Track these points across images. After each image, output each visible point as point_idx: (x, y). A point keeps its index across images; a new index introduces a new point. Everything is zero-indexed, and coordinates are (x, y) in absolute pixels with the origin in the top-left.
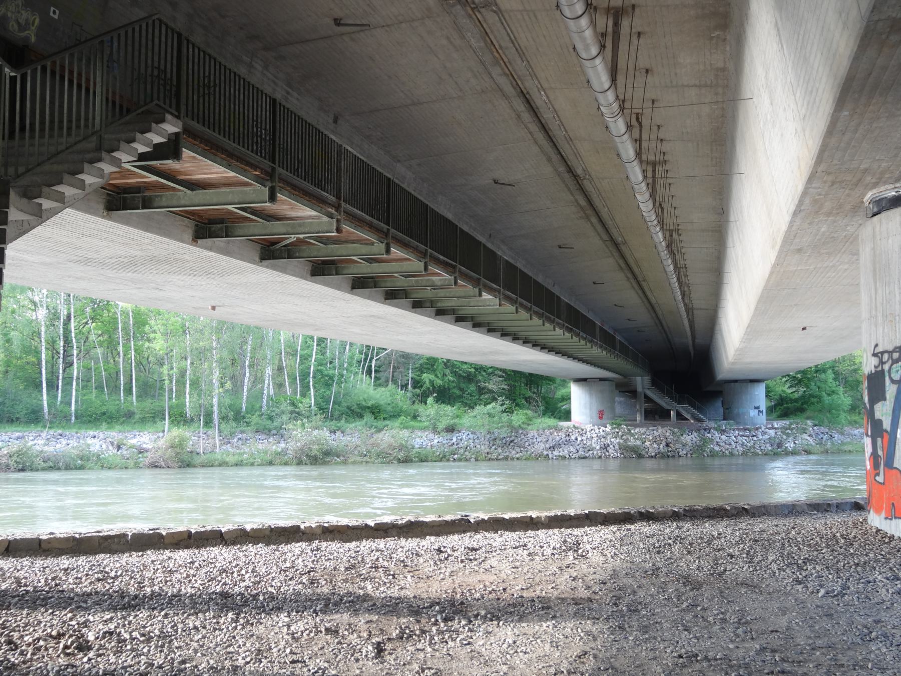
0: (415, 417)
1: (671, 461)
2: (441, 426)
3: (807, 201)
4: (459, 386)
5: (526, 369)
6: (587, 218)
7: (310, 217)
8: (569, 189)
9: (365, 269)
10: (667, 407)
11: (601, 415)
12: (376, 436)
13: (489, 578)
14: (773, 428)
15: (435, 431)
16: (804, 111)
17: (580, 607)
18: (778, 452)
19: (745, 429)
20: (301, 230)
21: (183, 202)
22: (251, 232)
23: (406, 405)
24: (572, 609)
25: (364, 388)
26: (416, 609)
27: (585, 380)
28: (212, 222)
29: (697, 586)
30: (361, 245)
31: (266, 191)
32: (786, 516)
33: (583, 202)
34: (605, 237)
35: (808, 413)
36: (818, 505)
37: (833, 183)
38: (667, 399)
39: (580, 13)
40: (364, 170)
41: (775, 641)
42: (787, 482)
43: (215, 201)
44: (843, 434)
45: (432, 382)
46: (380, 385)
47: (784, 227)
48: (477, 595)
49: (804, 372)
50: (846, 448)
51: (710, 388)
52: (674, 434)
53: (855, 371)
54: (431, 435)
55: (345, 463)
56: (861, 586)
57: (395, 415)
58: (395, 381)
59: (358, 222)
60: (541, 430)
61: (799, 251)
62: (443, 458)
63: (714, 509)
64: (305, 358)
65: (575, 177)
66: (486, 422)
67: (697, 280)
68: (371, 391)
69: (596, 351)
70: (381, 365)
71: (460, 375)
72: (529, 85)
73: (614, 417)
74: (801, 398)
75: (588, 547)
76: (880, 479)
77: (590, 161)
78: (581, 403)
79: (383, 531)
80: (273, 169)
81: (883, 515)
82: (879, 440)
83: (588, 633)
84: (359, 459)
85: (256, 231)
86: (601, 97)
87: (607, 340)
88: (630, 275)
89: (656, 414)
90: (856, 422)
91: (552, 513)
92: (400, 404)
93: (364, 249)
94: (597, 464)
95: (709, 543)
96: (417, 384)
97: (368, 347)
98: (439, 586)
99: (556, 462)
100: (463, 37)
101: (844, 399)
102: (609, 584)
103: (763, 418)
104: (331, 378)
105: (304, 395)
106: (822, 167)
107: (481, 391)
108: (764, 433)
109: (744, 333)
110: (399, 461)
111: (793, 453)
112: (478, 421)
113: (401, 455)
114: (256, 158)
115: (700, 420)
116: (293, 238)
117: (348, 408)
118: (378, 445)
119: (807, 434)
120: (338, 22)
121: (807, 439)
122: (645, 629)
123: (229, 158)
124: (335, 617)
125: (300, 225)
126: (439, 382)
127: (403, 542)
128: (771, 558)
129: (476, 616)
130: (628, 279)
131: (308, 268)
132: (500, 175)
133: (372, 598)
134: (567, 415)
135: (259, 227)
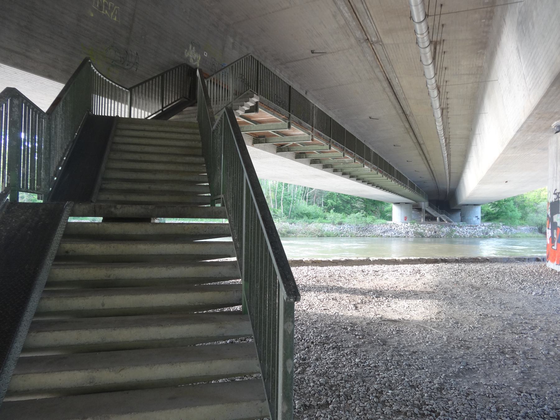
0: (325, 218)
1: (437, 239)
2: (336, 222)
3: (525, 126)
4: (343, 205)
5: (373, 198)
6: (409, 133)
7: (300, 134)
8: (402, 121)
9: (317, 155)
10: (435, 216)
11: (406, 219)
12: (309, 226)
13: (388, 282)
14: (484, 226)
15: (334, 224)
16: (530, 87)
17: (430, 295)
18: (486, 236)
19: (471, 226)
20: (297, 140)
21: (252, 129)
22: (276, 141)
23: (321, 213)
24: (428, 296)
25: (303, 206)
26: (364, 293)
27: (399, 203)
28: (260, 137)
29: (478, 289)
30: (321, 146)
31: (287, 124)
32: (506, 263)
33: (407, 126)
34: (415, 141)
35: (500, 219)
36: (520, 258)
37: (539, 118)
38: (435, 212)
39: (427, 45)
40: (321, 114)
41: (519, 311)
42: (488, 249)
43: (265, 128)
44: (516, 229)
45: (332, 204)
46: (310, 204)
47: (510, 137)
48: (386, 289)
49: (499, 201)
50: (518, 235)
51: (455, 208)
52: (438, 227)
53: (524, 201)
54: (332, 226)
55: (296, 236)
56: (550, 292)
57: (316, 217)
58: (316, 203)
59: (319, 136)
60: (379, 225)
61: (515, 147)
62: (337, 235)
63: (474, 259)
64: (279, 193)
65: (406, 115)
66: (356, 221)
67: (455, 160)
68: (306, 207)
69: (407, 191)
70: (310, 196)
71: (344, 201)
72: (391, 76)
73: (412, 219)
74: (498, 213)
75: (425, 272)
76: (555, 247)
77: (415, 109)
78: (397, 213)
79: (335, 263)
80: (290, 115)
81: (555, 263)
82: (555, 231)
83: (438, 305)
84: (302, 235)
85: (278, 141)
86: (429, 82)
87: (412, 186)
88: (424, 158)
89: (430, 218)
90: (523, 224)
91: (404, 258)
92: (319, 212)
93: (320, 147)
94: (403, 239)
95: (477, 272)
96: (325, 204)
97: (305, 187)
98: (367, 285)
99: (385, 239)
100: (365, 56)
101: (518, 213)
102: (440, 287)
103: (479, 221)
104: (290, 201)
105: (278, 208)
106: (536, 111)
107: (353, 207)
108: (479, 228)
109: (475, 184)
110: (318, 236)
111: (493, 237)
112: (352, 220)
113: (319, 234)
114: (283, 110)
115: (450, 222)
116: (291, 143)
117: (297, 214)
118: (310, 230)
119: (500, 228)
120: (313, 52)
121: (500, 231)
122: (461, 304)
123: (274, 111)
124: (334, 294)
125: (296, 138)
126: (335, 203)
127: (347, 267)
128: (506, 279)
129: (388, 296)
130: (423, 159)
131: (294, 155)
132: (372, 115)
133: (344, 288)
134: (390, 218)
135: (279, 139)
